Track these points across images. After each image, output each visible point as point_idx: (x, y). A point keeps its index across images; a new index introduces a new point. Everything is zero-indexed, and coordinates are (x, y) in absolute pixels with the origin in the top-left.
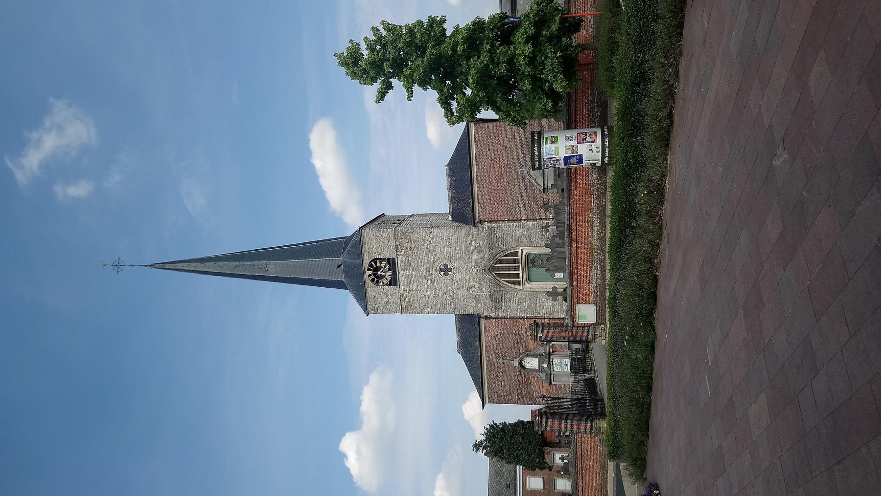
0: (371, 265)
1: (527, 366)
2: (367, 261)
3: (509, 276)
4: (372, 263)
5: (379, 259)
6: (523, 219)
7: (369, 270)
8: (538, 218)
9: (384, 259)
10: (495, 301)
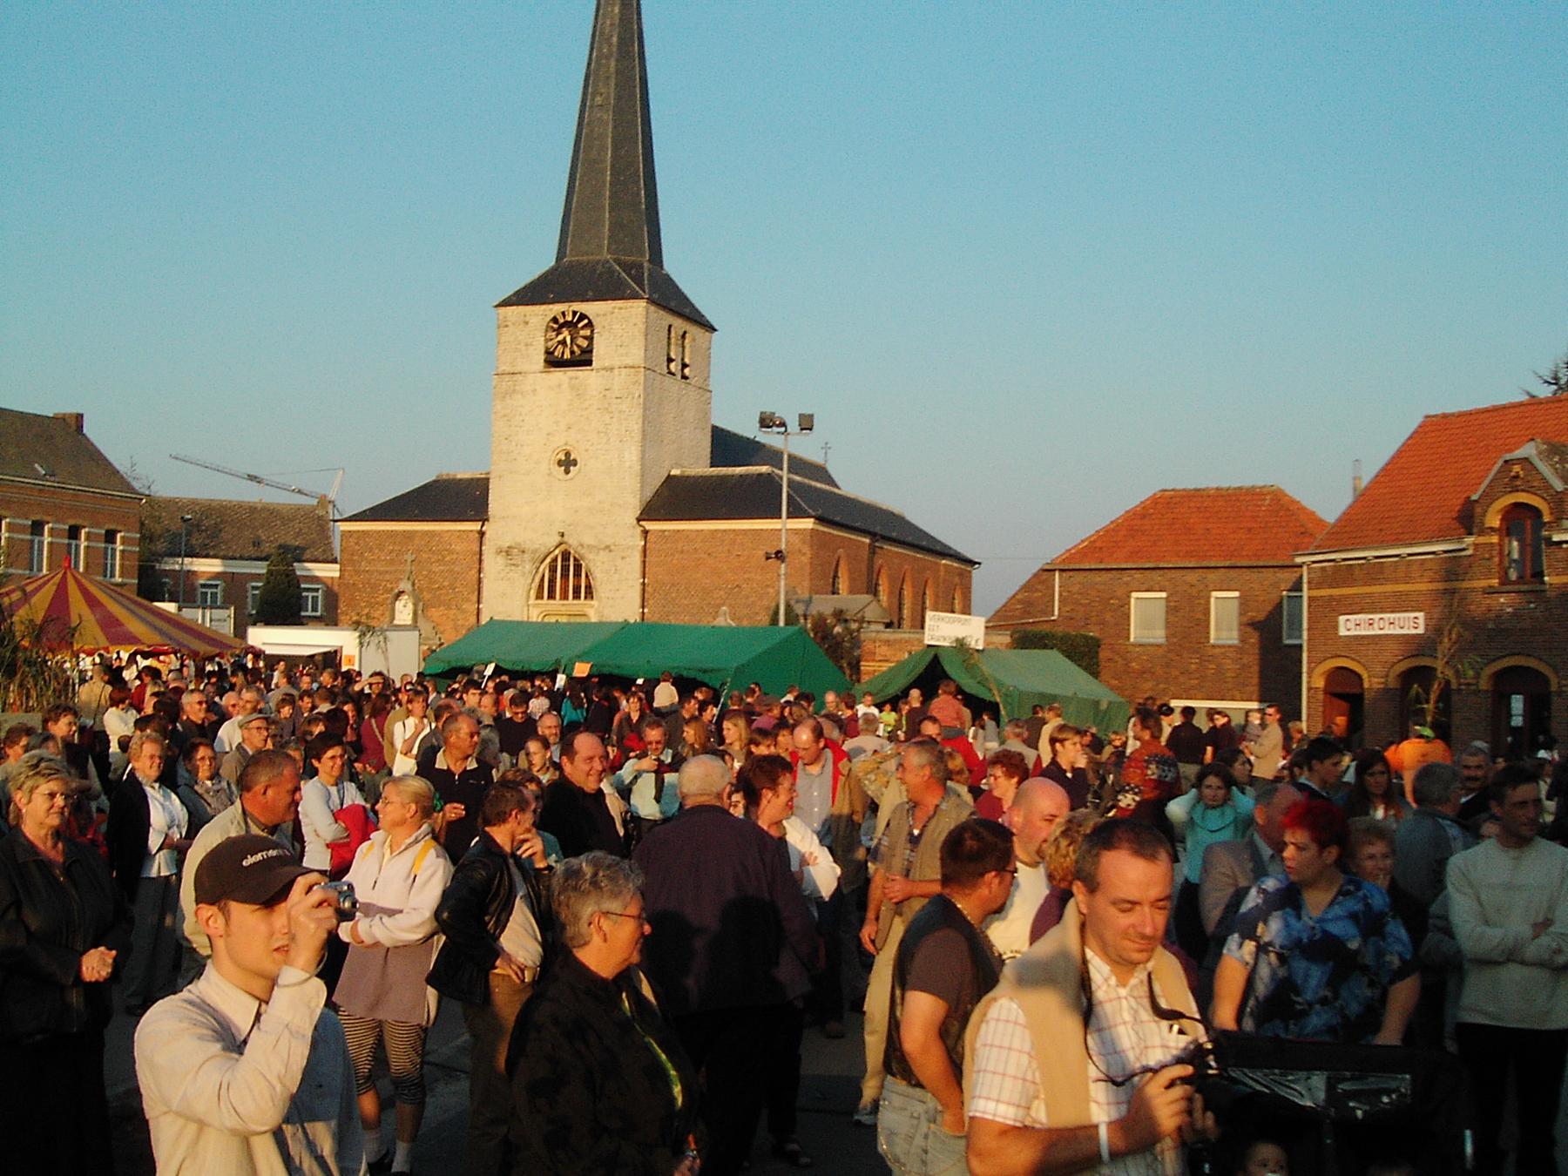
0: (583, 317)
1: (399, 605)
2: (589, 308)
3: (552, 581)
4: (586, 321)
5: (590, 322)
6: (646, 610)
7: (575, 313)
8: (646, 610)
9: (590, 339)
10: (508, 552)
